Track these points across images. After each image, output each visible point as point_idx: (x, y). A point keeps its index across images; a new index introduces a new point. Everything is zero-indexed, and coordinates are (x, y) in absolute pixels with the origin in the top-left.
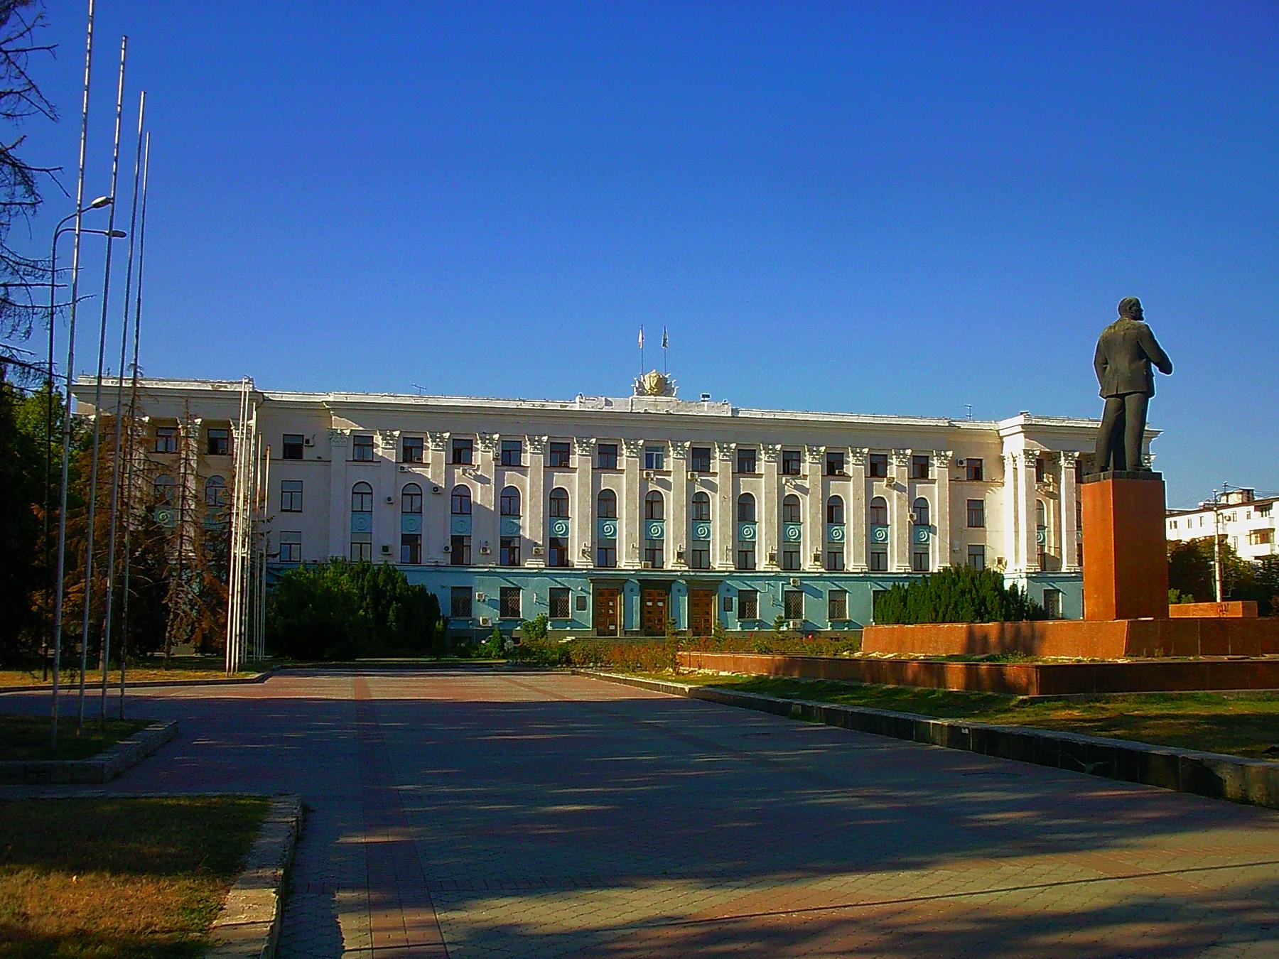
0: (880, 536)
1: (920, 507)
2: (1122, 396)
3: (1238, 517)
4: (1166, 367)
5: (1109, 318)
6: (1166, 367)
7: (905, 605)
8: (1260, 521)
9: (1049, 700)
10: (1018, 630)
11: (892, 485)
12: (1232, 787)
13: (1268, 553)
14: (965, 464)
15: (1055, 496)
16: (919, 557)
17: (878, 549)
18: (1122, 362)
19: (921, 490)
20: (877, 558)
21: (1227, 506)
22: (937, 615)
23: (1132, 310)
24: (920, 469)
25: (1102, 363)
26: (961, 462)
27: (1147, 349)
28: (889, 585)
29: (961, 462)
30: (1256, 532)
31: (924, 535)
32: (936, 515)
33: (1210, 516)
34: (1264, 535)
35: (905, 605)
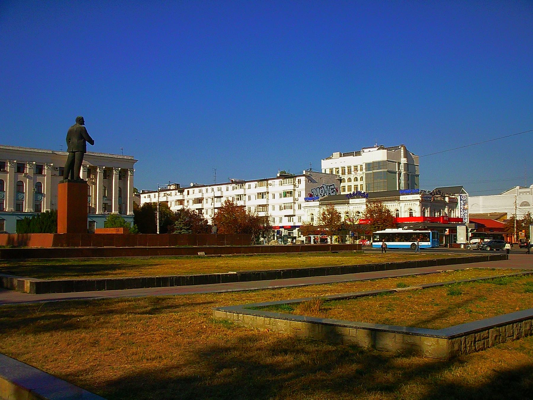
0: (20, 197)
1: (38, 186)
2: (74, 152)
3: (195, 192)
4: (92, 142)
5: (72, 124)
6: (92, 142)
7: (29, 226)
8: (179, 197)
9: (3, 261)
10: (23, 236)
11: (27, 176)
12: (5, 285)
13: (220, 206)
14: (58, 169)
15: (95, 184)
16: (37, 207)
17: (19, 202)
18: (75, 140)
19: (39, 179)
20: (19, 206)
21: (170, 190)
22: (42, 229)
23: (81, 121)
24: (39, 170)
25: (69, 140)
26: (57, 168)
27: (84, 136)
28: (23, 217)
29: (57, 168)
30: (178, 200)
31: (39, 197)
32: (45, 189)
33: (197, 190)
34: (181, 202)
35: (29, 226)
